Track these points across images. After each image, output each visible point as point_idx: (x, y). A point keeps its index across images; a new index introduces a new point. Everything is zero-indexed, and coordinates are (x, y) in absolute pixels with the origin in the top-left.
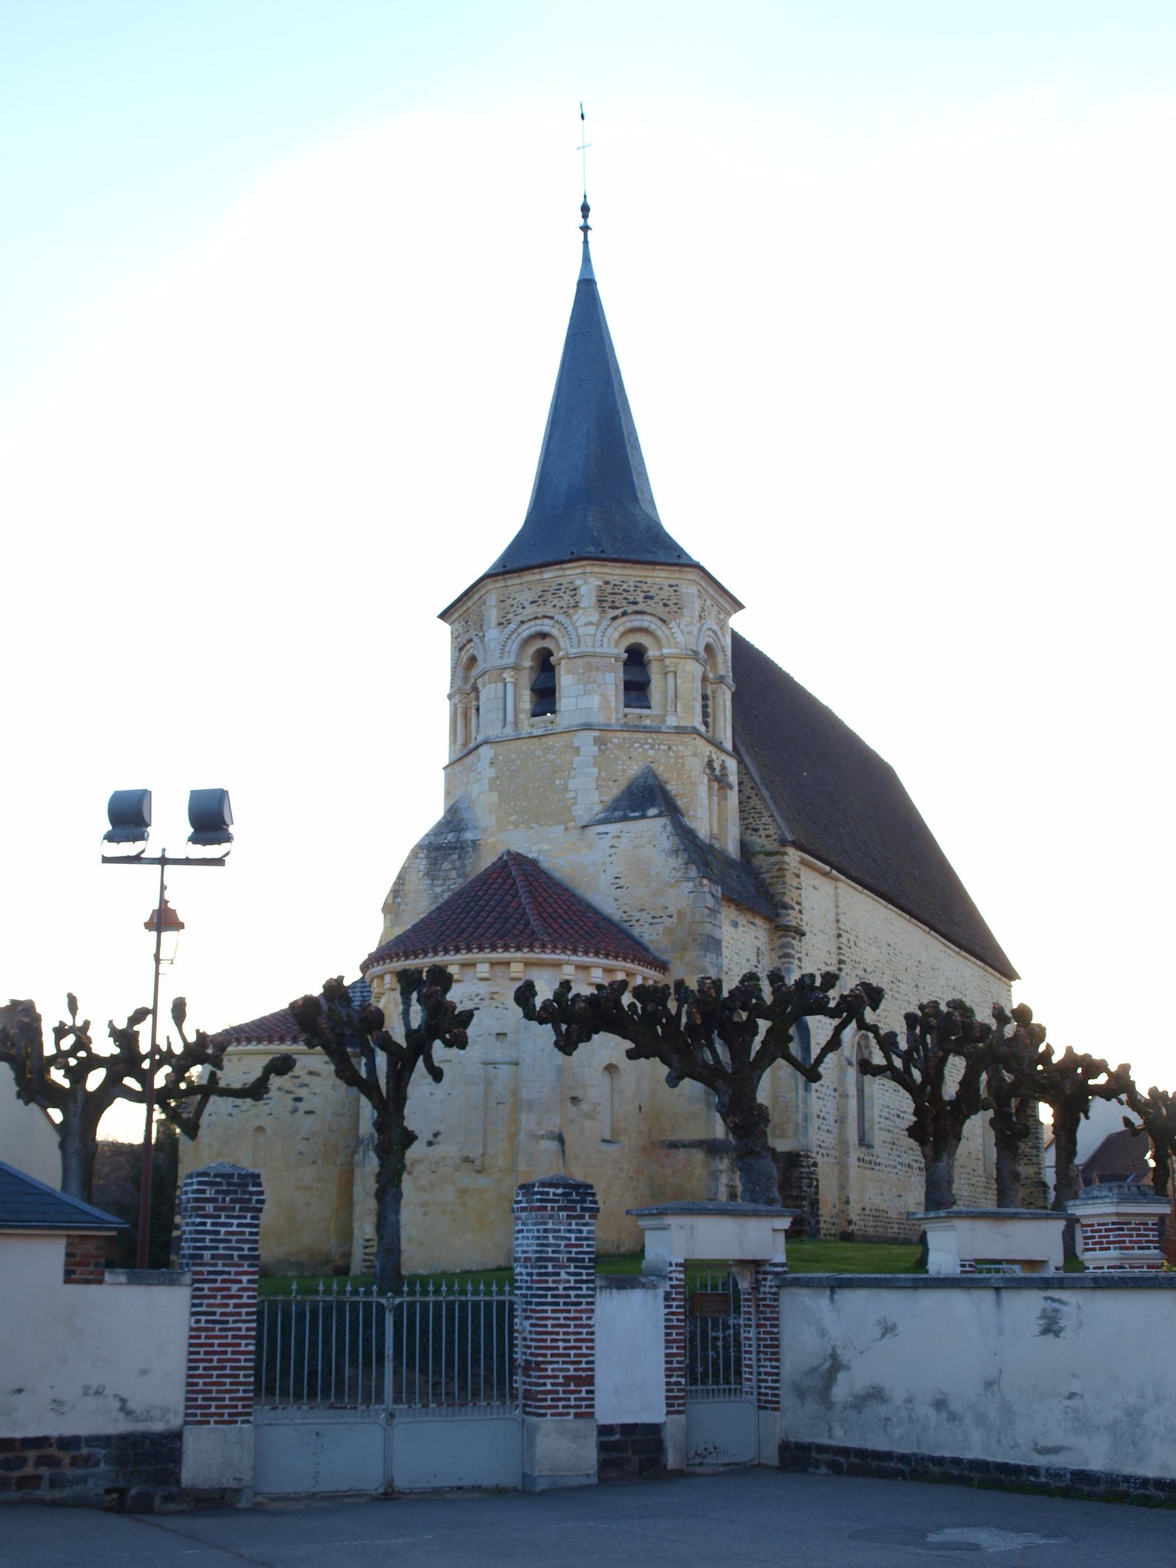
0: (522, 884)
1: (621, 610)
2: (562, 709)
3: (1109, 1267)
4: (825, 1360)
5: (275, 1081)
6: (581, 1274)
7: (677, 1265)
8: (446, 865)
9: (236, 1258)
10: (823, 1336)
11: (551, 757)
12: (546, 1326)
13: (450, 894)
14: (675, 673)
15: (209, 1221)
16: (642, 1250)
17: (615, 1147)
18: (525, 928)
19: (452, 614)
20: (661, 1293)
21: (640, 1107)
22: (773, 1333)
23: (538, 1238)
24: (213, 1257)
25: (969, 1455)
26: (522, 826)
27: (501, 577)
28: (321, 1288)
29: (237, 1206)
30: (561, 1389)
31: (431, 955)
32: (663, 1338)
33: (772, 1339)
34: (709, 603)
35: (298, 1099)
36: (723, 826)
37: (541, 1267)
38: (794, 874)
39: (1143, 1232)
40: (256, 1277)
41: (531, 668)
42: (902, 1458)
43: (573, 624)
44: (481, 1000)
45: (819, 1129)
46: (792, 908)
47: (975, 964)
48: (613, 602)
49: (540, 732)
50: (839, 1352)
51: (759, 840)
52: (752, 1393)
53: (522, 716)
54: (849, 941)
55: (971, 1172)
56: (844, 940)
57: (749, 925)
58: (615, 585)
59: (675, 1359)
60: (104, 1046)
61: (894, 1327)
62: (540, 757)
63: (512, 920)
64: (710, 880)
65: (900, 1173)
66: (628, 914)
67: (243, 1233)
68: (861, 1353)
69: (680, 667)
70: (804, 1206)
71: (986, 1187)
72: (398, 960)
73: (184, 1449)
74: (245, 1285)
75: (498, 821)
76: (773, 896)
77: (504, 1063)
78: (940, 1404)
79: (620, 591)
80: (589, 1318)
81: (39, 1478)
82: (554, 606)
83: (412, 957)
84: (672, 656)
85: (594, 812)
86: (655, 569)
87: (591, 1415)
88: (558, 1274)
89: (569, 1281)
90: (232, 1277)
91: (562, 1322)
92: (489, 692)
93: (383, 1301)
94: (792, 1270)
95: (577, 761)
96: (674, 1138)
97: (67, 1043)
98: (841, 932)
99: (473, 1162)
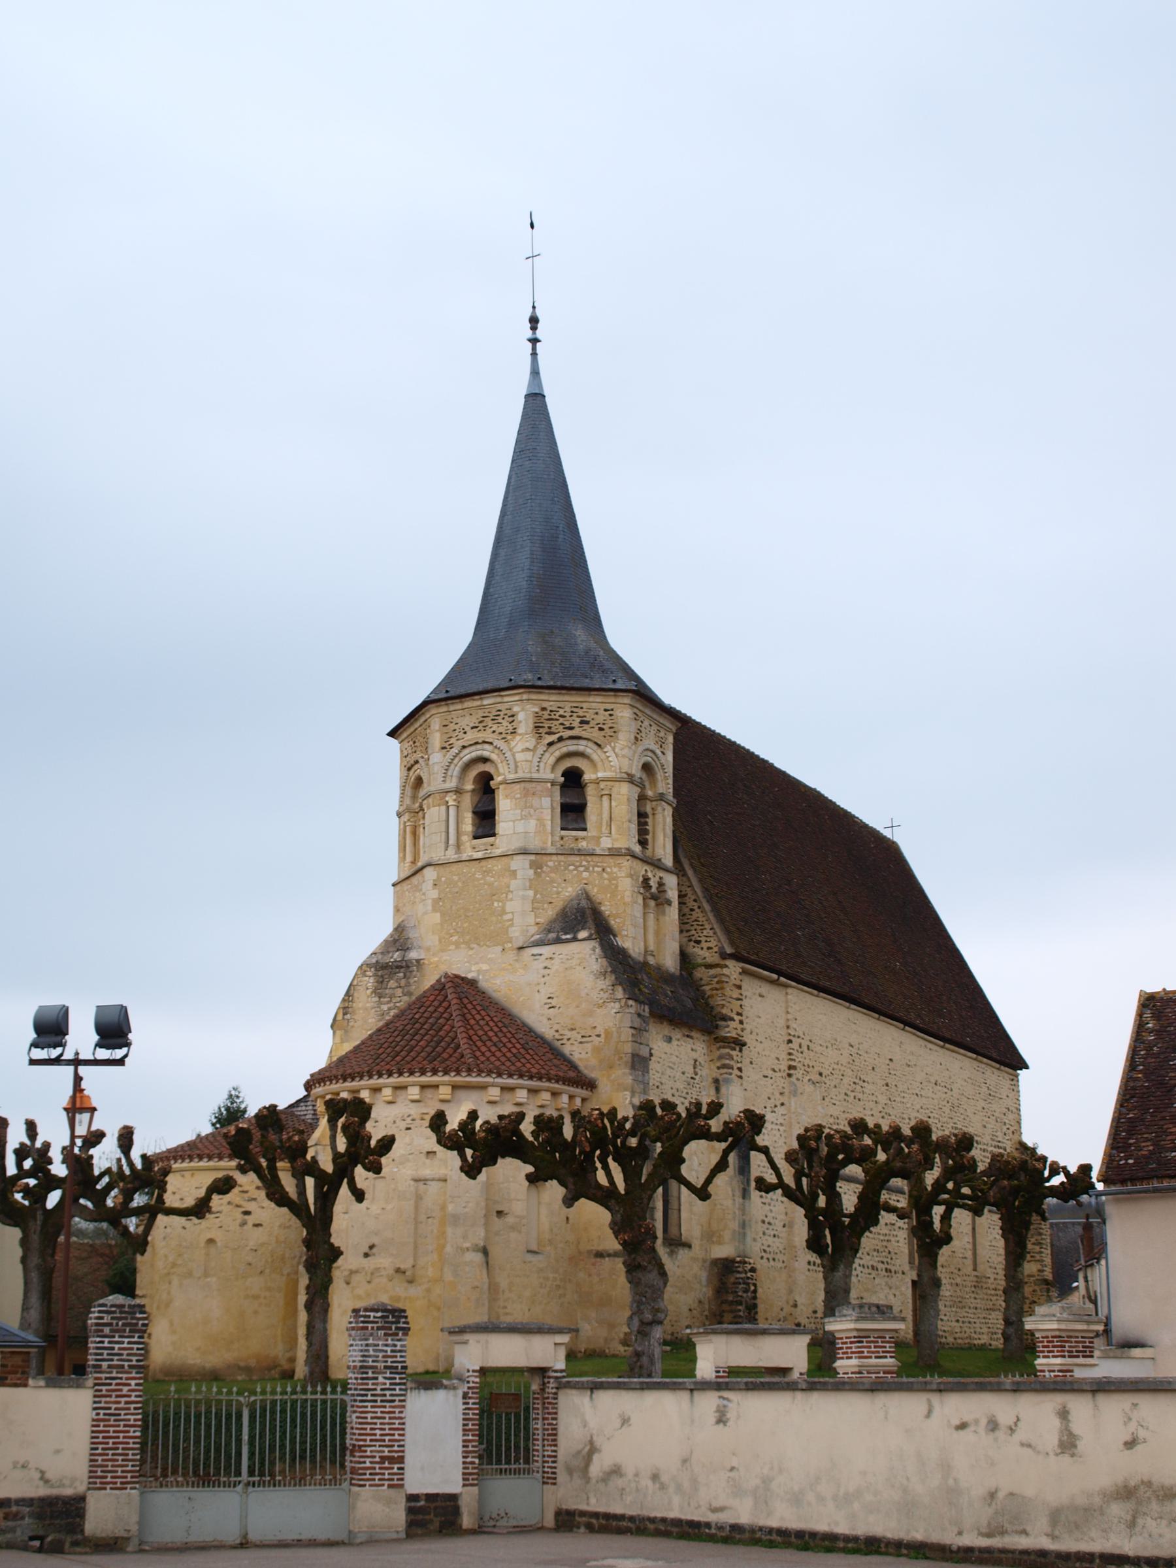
1: (557, 736)
2: (501, 833)
3: (852, 1373)
4: (586, 1445)
5: (216, 1201)
7: (473, 1371)
8: (392, 984)
9: (126, 1367)
11: (490, 879)
12: (366, 1418)
15: (107, 1340)
17: (540, 1257)
18: (455, 1051)
20: (460, 1393)
21: (567, 1218)
22: (552, 1424)
23: (362, 1351)
24: (109, 1366)
25: (672, 1515)
26: (463, 946)
27: (443, 703)
28: (259, 1390)
30: (377, 1466)
31: (366, 1078)
32: (461, 1427)
33: (552, 1429)
34: (646, 723)
35: (247, 1213)
36: (659, 942)
37: (363, 1373)
38: (735, 985)
39: (880, 1344)
40: (141, 1381)
41: (473, 791)
42: (632, 1519)
44: (413, 1120)
45: (764, 1233)
47: (965, 1056)
48: (550, 728)
49: (479, 855)
50: (595, 1438)
51: (701, 952)
52: (538, 1472)
53: (465, 838)
54: (800, 1047)
55: (956, 1271)
56: (795, 1045)
57: (685, 1038)
59: (470, 1444)
60: (59, 1169)
61: (629, 1419)
62: (479, 880)
63: (443, 1044)
64: (636, 1001)
65: (860, 1274)
67: (132, 1349)
71: (975, 1287)
72: (337, 1082)
73: (87, 1508)
74: (133, 1387)
75: (440, 941)
77: (433, 1180)
78: (655, 1477)
79: (557, 717)
80: (401, 1412)
82: (494, 732)
83: (349, 1080)
84: (604, 780)
85: (530, 934)
86: (590, 695)
87: (402, 1486)
88: (377, 1378)
89: (385, 1384)
90: (124, 1381)
91: (379, 1415)
92: (434, 814)
93: (241, 1399)
94: (568, 1376)
95: (514, 884)
96: (600, 1248)
97: (28, 1164)
98: (791, 1038)
99: (404, 1272)
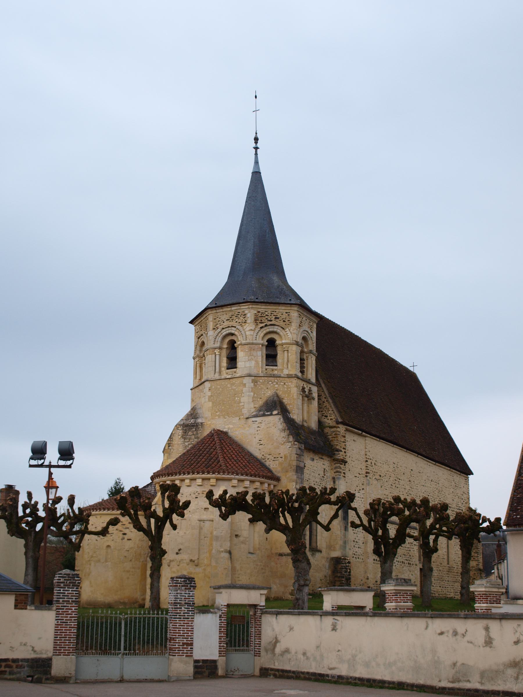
0: (218, 444)
1: (265, 324)
3: (393, 609)
5: (111, 528)
6: (189, 608)
7: (224, 606)
8: (190, 433)
9: (70, 602)
10: (273, 631)
11: (234, 387)
12: (176, 626)
13: (192, 445)
14: (288, 351)
15: (62, 589)
16: (145, 604)
17: (254, 555)
19: (195, 322)
20: (218, 615)
21: (267, 538)
22: (259, 630)
23: (175, 596)
28: (129, 612)
29: (71, 585)
30: (181, 647)
32: (218, 631)
33: (259, 632)
34: (304, 319)
35: (125, 534)
38: (342, 436)
40: (77, 608)
41: (227, 348)
42: (294, 672)
43: (244, 330)
44: (198, 494)
45: (354, 546)
46: (341, 451)
48: (261, 320)
49: (229, 377)
50: (278, 636)
52: (252, 651)
53: (223, 369)
55: (439, 564)
56: (369, 463)
57: (320, 459)
58: (262, 313)
59: (222, 638)
60: (42, 513)
61: (293, 628)
62: (229, 387)
63: (212, 460)
64: (298, 442)
66: (264, 456)
68: (284, 637)
69: (290, 348)
70: (343, 580)
73: (52, 663)
74: (73, 610)
75: (212, 414)
76: (332, 446)
77: (207, 521)
78: (304, 654)
79: (264, 316)
80: (192, 623)
81: (6, 671)
82: (236, 322)
87: (192, 656)
88: (181, 608)
89: (185, 611)
91: (182, 624)
92: (209, 358)
93: (121, 616)
95: (245, 390)
96: (281, 552)
99: (194, 561)
